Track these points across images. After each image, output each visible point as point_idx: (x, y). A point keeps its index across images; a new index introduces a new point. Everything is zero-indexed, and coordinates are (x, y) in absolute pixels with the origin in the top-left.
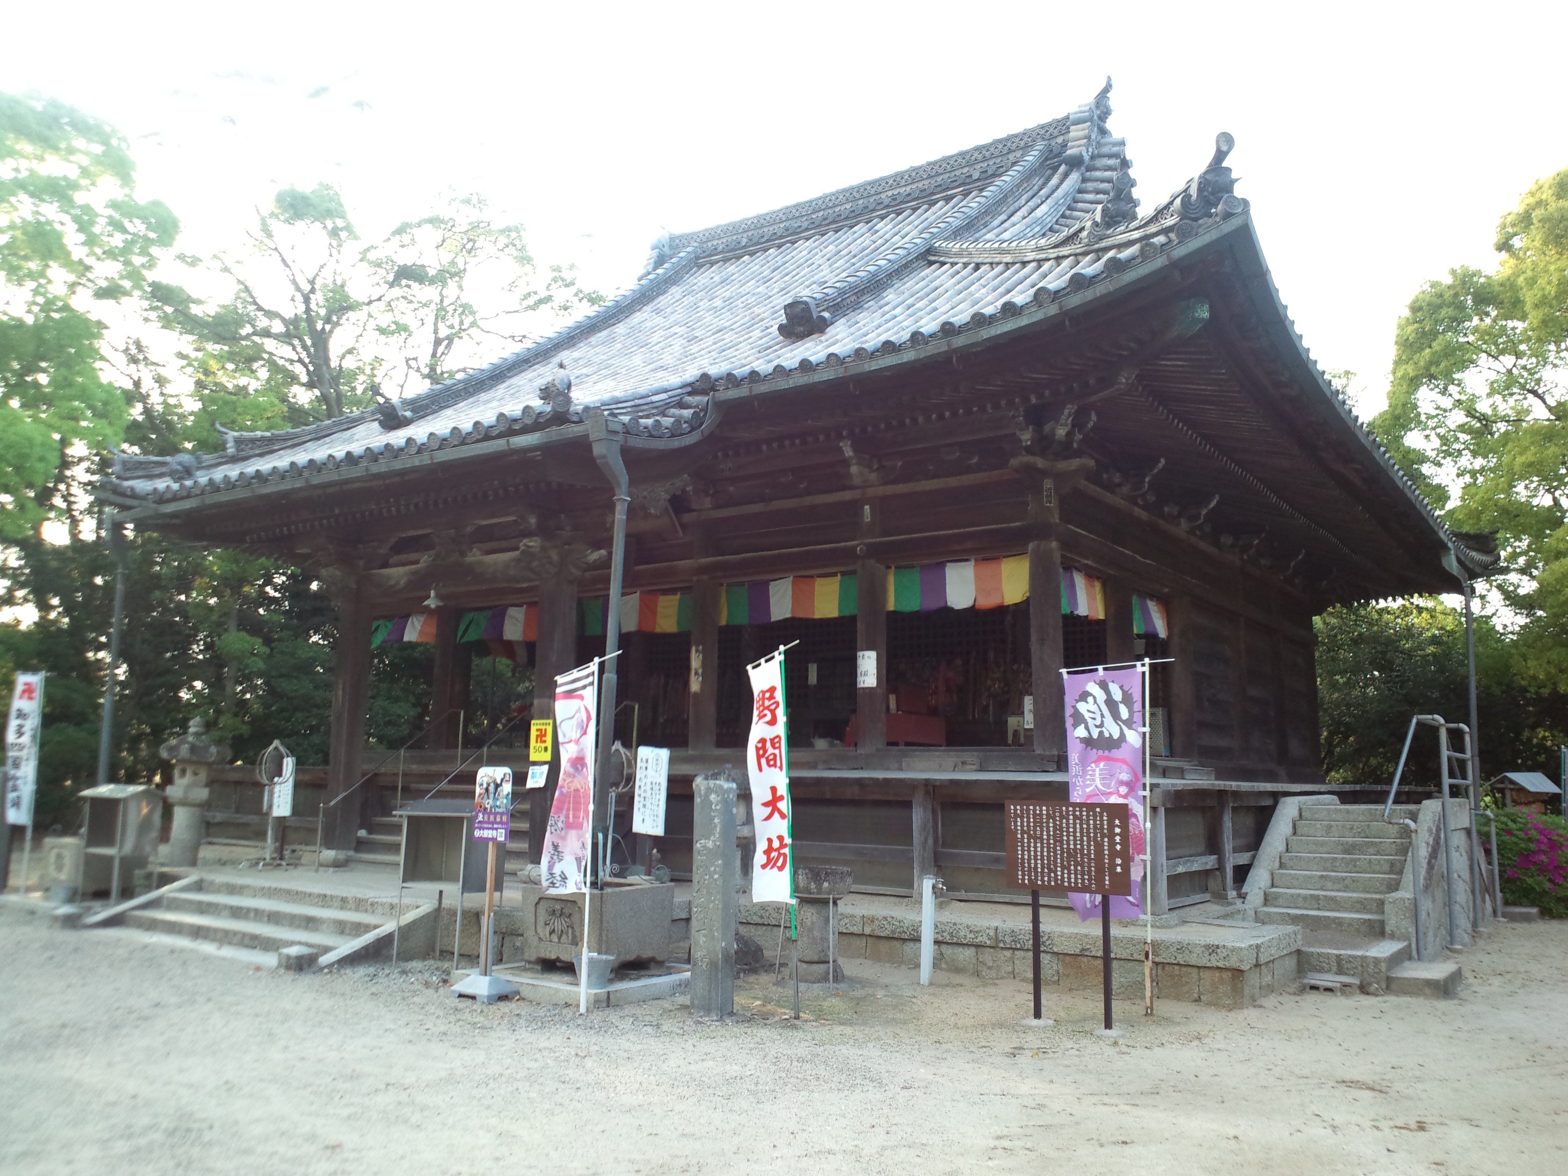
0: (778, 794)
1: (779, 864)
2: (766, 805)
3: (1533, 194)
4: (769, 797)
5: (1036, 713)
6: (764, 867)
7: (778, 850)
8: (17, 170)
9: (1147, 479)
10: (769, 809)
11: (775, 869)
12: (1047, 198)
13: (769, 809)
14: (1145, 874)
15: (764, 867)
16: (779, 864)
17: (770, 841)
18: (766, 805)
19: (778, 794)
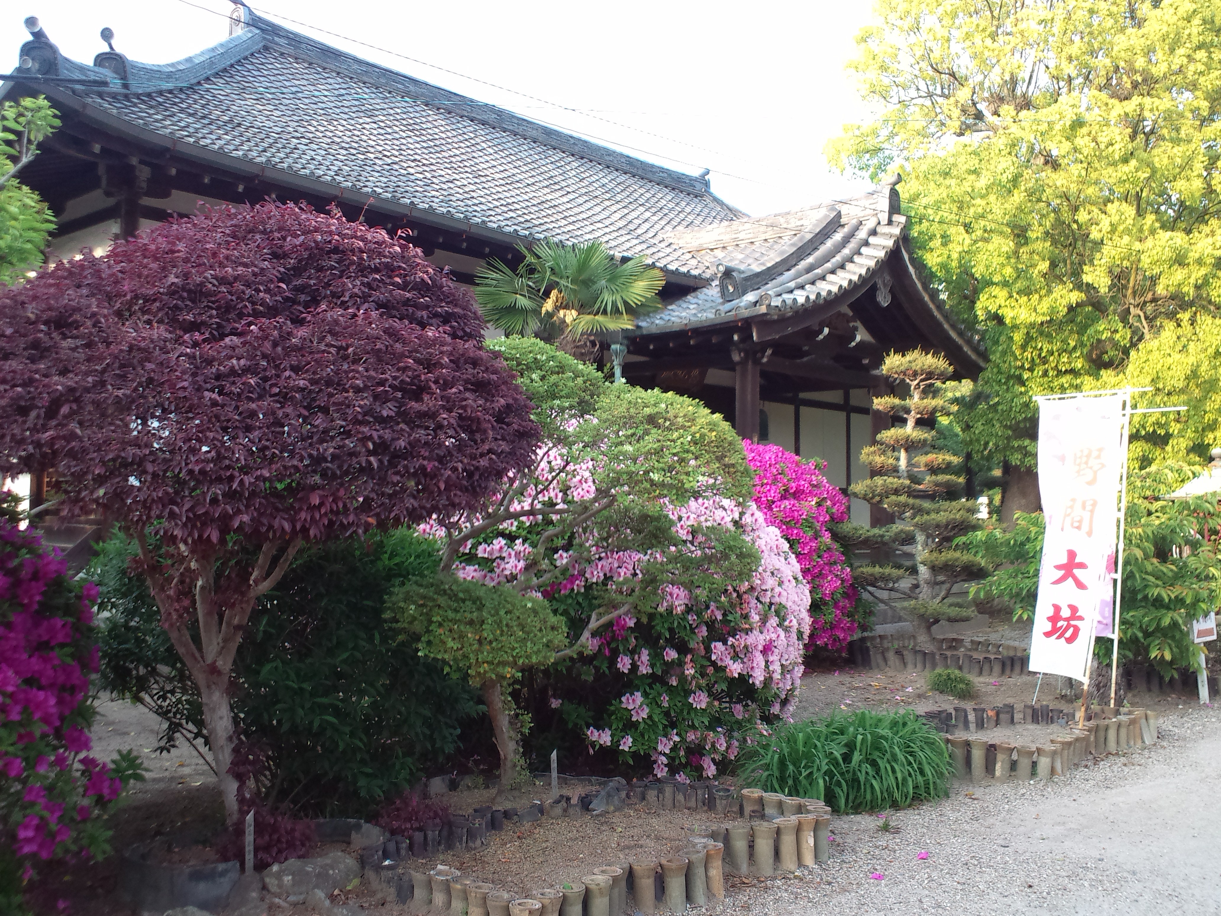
0: (1077, 560)
1: (1068, 634)
2: (1058, 567)
3: (1078, 388)
4: (1064, 560)
5: (758, 333)
6: (1048, 634)
7: (1067, 620)
8: (1070, 567)
9: (200, 583)
10: (1062, 573)
11: (1063, 640)
12: (751, 847)
13: (1062, 573)
14: (1117, 551)
15: (1048, 634)
16: (1068, 634)
17: (1057, 608)
18: (1058, 567)
19: (1077, 560)
